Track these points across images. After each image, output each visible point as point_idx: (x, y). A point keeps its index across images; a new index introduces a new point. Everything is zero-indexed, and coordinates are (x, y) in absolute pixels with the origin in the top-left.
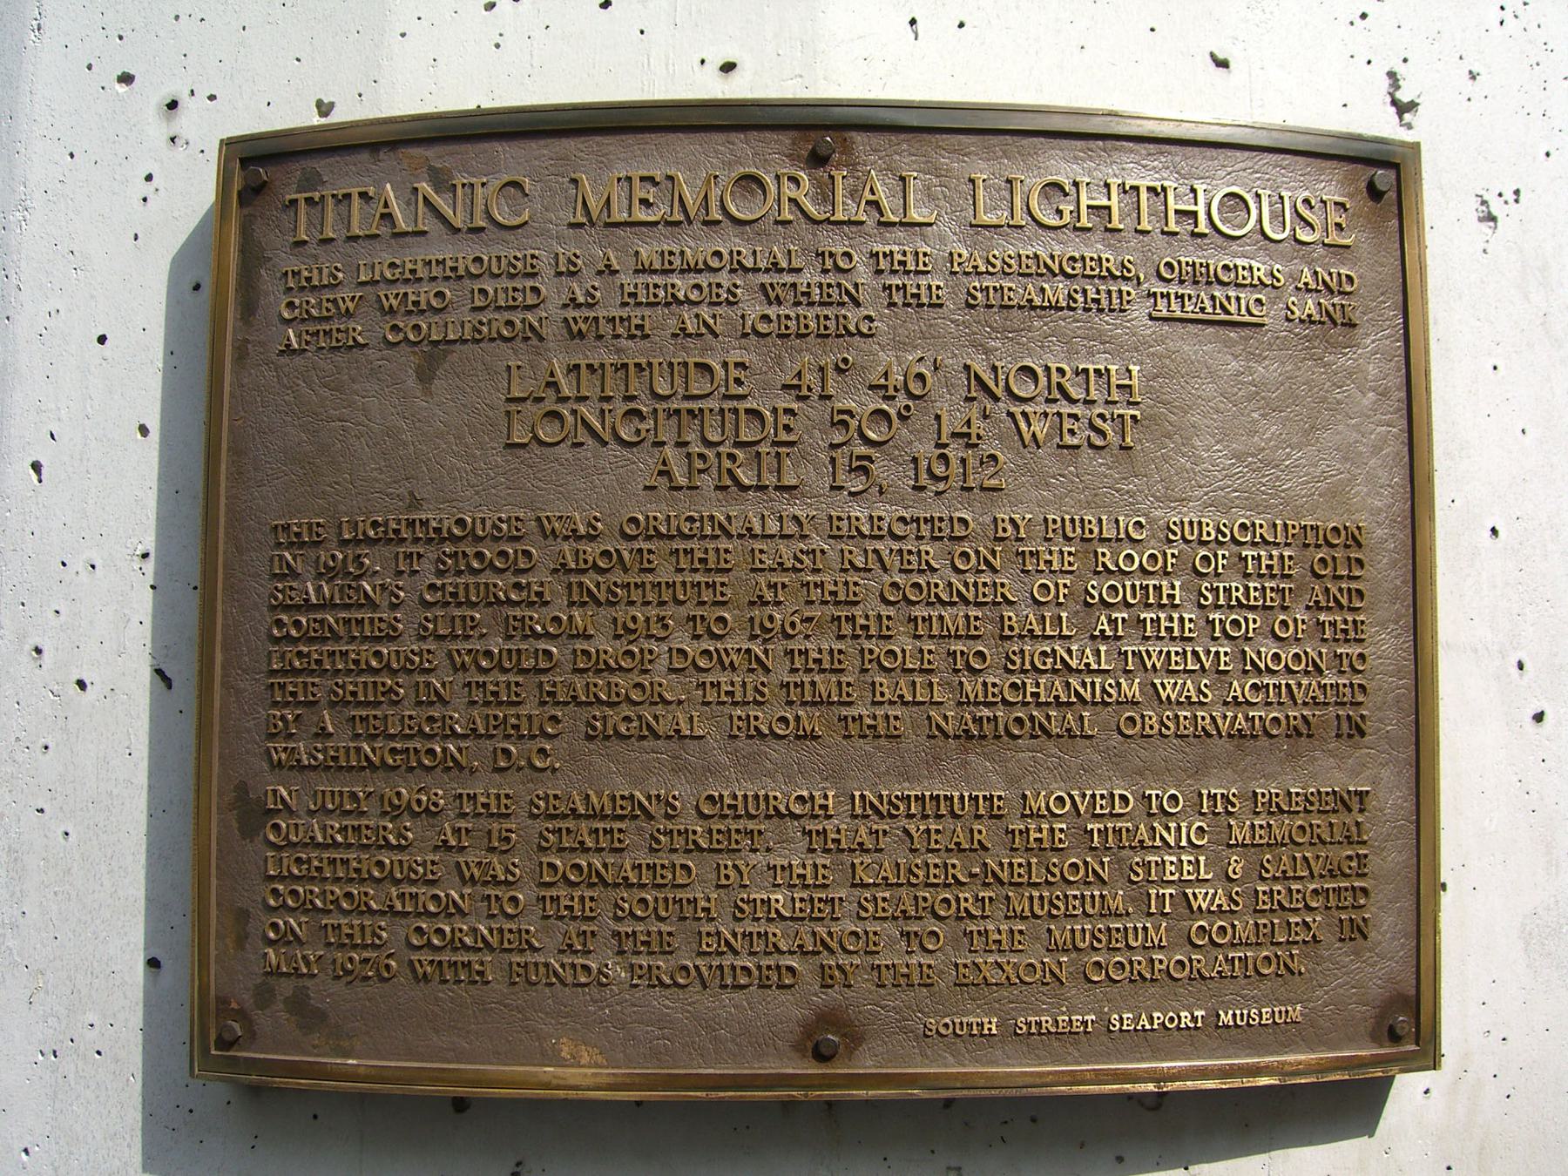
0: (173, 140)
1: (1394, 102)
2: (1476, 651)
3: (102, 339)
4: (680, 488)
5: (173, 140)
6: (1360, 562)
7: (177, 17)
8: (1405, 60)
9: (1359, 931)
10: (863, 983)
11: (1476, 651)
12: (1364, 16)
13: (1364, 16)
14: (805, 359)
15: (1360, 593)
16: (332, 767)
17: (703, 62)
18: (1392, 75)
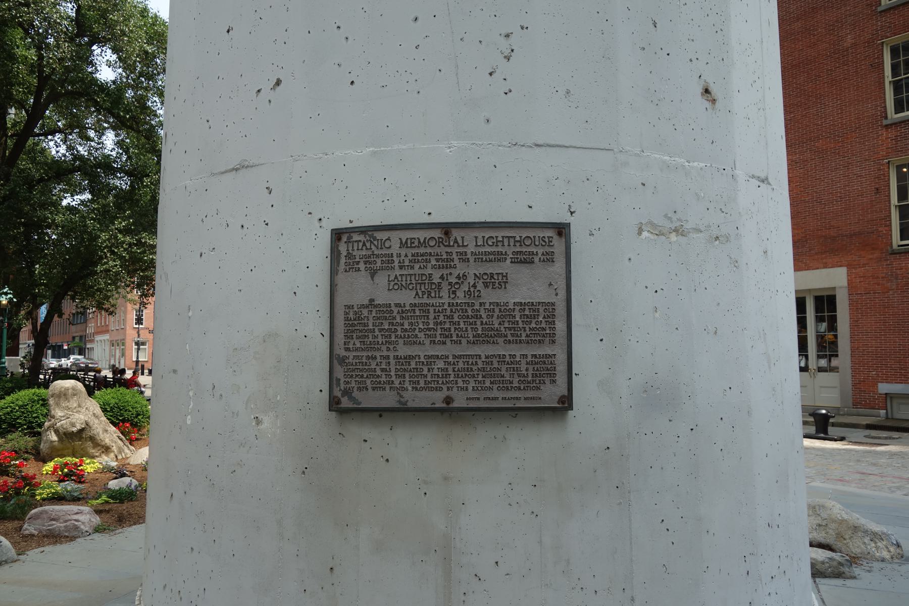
10: (455, 389)
14: (445, 272)
16: (357, 350)
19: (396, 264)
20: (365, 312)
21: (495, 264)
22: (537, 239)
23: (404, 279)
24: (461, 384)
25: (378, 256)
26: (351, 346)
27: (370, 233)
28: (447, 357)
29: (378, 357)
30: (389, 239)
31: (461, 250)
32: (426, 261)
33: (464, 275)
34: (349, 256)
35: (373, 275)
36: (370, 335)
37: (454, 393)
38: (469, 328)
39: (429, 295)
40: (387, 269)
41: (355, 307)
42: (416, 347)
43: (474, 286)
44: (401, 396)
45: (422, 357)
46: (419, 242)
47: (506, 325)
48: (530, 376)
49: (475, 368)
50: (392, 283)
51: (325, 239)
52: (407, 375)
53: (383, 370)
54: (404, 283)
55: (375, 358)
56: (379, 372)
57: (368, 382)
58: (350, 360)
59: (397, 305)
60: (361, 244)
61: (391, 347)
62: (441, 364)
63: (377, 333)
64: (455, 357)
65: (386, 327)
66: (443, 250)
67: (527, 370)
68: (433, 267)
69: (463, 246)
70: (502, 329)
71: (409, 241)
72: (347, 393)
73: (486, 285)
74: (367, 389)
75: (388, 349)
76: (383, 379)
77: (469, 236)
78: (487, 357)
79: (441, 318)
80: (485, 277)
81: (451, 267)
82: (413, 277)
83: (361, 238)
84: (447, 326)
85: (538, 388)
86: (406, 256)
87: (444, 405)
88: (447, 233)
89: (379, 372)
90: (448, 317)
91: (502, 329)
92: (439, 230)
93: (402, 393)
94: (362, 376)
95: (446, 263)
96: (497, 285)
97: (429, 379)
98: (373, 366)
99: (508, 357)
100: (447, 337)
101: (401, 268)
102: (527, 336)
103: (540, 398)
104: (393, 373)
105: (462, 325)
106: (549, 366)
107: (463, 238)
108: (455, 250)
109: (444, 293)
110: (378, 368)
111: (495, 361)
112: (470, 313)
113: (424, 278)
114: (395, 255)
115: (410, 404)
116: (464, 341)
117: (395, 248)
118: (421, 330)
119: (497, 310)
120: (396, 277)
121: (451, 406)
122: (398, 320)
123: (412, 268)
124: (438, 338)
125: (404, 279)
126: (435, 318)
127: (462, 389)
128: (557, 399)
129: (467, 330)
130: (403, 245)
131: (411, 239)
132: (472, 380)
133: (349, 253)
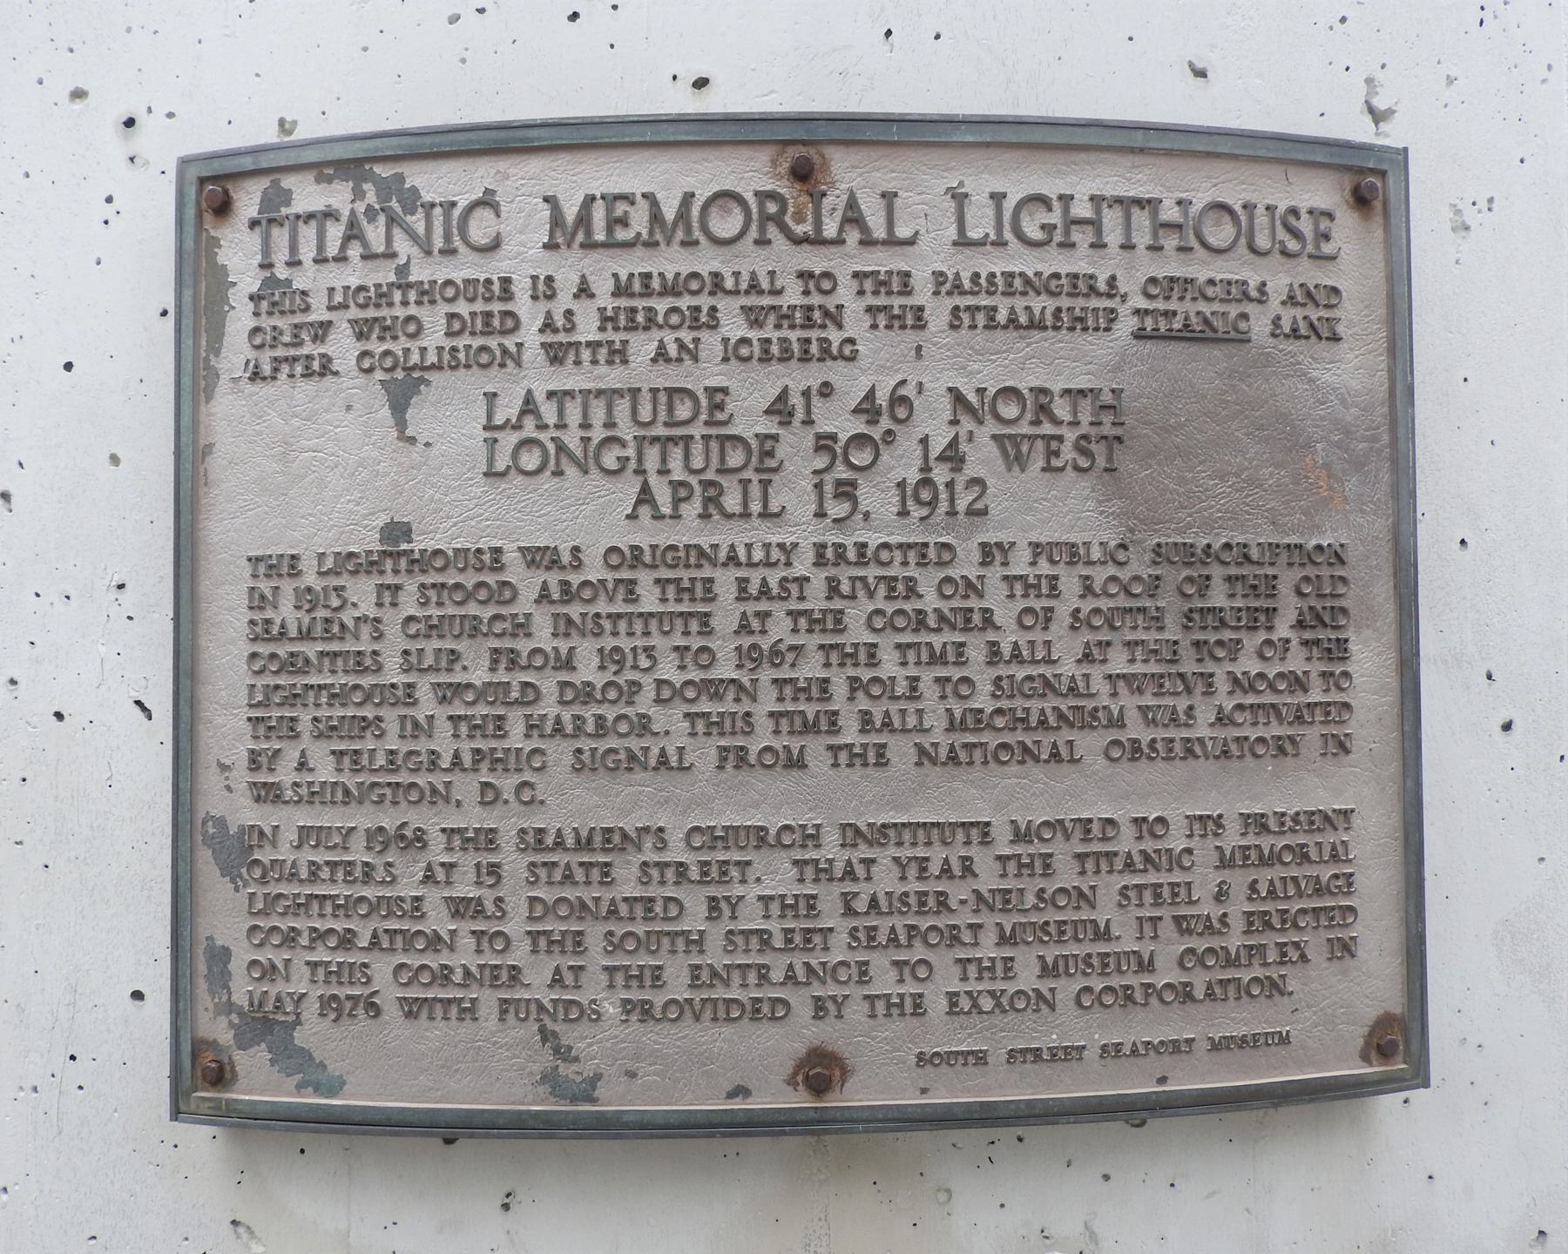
0: (132, 159)
1: (1371, 110)
2: (1445, 662)
3: (68, 366)
4: (663, 517)
5: (132, 159)
6: (1343, 579)
7: (129, 30)
8: (1383, 67)
9: (1346, 948)
10: (856, 1011)
11: (1445, 662)
12: (1343, 20)
13: (1343, 20)
14: (812, 376)
15: (1344, 611)
16: (315, 796)
17: (675, 78)
18: (1369, 81)
19: (530, 335)
20: (362, 593)
21: (1062, 343)
22: (1261, 218)
23: (574, 414)
24: (885, 982)
25: (427, 294)
26: (285, 774)
27: (383, 171)
28: (812, 838)
29: (437, 841)
30: (487, 201)
31: (882, 261)
32: (694, 319)
33: (898, 400)
34: (273, 295)
35: (403, 390)
36: (391, 716)
37: (851, 1034)
38: (927, 676)
39: (713, 501)
40: (481, 361)
41: (308, 565)
42: (642, 785)
43: (953, 456)
44: (563, 1053)
45: (676, 837)
46: (656, 217)
47: (1118, 663)
48: (1237, 924)
49: (958, 892)
50: (509, 440)
51: (154, 208)
52: (595, 934)
53: (460, 908)
54: (572, 439)
55: (419, 840)
56: (438, 920)
57: (382, 968)
58: (285, 853)
59: (539, 557)
60: (335, 232)
61: (507, 784)
62: (778, 875)
63: (428, 705)
64: (852, 834)
65: (479, 675)
66: (782, 261)
67: (1221, 896)
68: (734, 352)
69: (892, 242)
70: (1100, 685)
71: (599, 214)
72: (266, 1024)
73: (1013, 451)
74: (374, 1010)
75: (489, 796)
76: (465, 957)
77: (922, 192)
78: (1021, 835)
79: (779, 629)
80: (1009, 410)
81: (826, 353)
82: (623, 407)
83: (338, 196)
84: (810, 668)
85: (1275, 988)
86: (584, 291)
87: (799, 1100)
88: (803, 174)
89: (438, 920)
90: (815, 623)
91: (1100, 685)
92: (763, 156)
93: (570, 1036)
94: (347, 941)
95: (806, 331)
96: (1068, 453)
97: (715, 957)
98: (408, 888)
99: (1128, 831)
100: (810, 728)
101: (555, 354)
102: (1222, 719)
103: (1284, 1040)
104: (515, 926)
105: (889, 666)
106: (1326, 873)
107: (889, 197)
108: (846, 262)
109: (794, 492)
110: (434, 898)
111: (1062, 852)
112: (930, 601)
113: (683, 411)
114: (521, 288)
115: (613, 1100)
116: (901, 750)
117: (524, 253)
118: (667, 694)
119: (1070, 584)
120: (529, 406)
121: (833, 1101)
122: (543, 636)
123: (619, 355)
124: (763, 738)
125: (574, 414)
126: (744, 628)
127: (894, 1007)
128: (1356, 1035)
129: (914, 693)
130: (568, 231)
131: (612, 199)
132: (944, 960)
133: (271, 282)
